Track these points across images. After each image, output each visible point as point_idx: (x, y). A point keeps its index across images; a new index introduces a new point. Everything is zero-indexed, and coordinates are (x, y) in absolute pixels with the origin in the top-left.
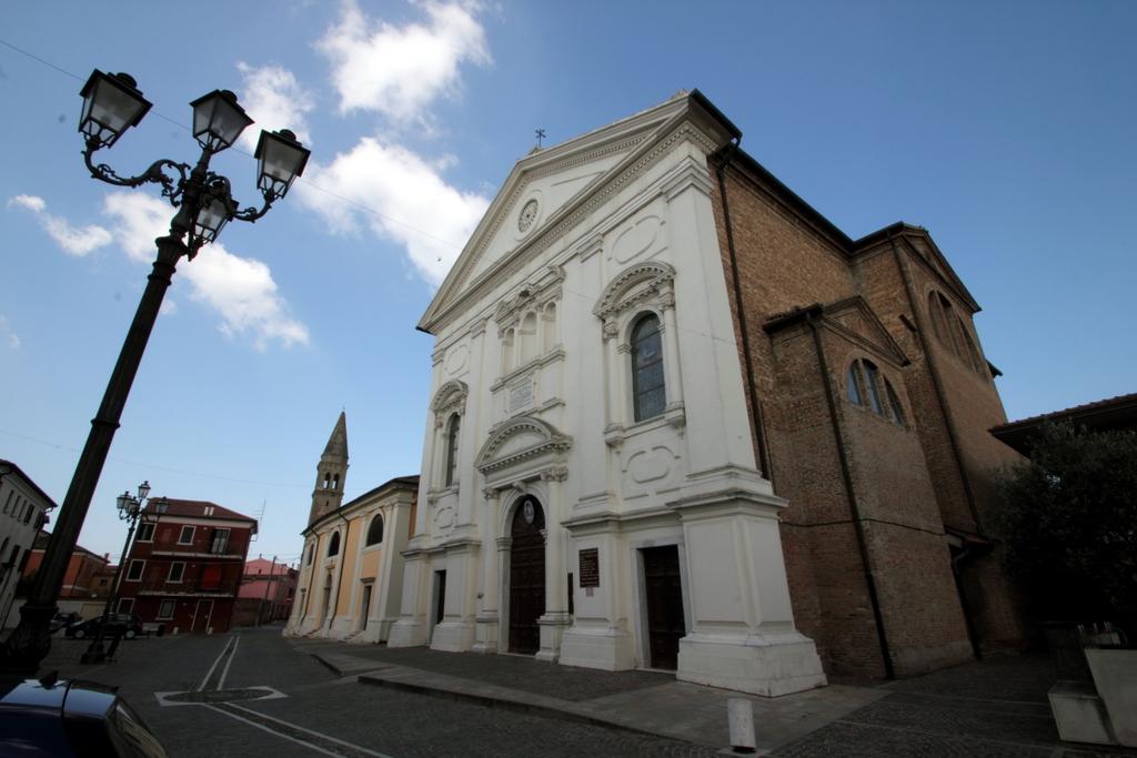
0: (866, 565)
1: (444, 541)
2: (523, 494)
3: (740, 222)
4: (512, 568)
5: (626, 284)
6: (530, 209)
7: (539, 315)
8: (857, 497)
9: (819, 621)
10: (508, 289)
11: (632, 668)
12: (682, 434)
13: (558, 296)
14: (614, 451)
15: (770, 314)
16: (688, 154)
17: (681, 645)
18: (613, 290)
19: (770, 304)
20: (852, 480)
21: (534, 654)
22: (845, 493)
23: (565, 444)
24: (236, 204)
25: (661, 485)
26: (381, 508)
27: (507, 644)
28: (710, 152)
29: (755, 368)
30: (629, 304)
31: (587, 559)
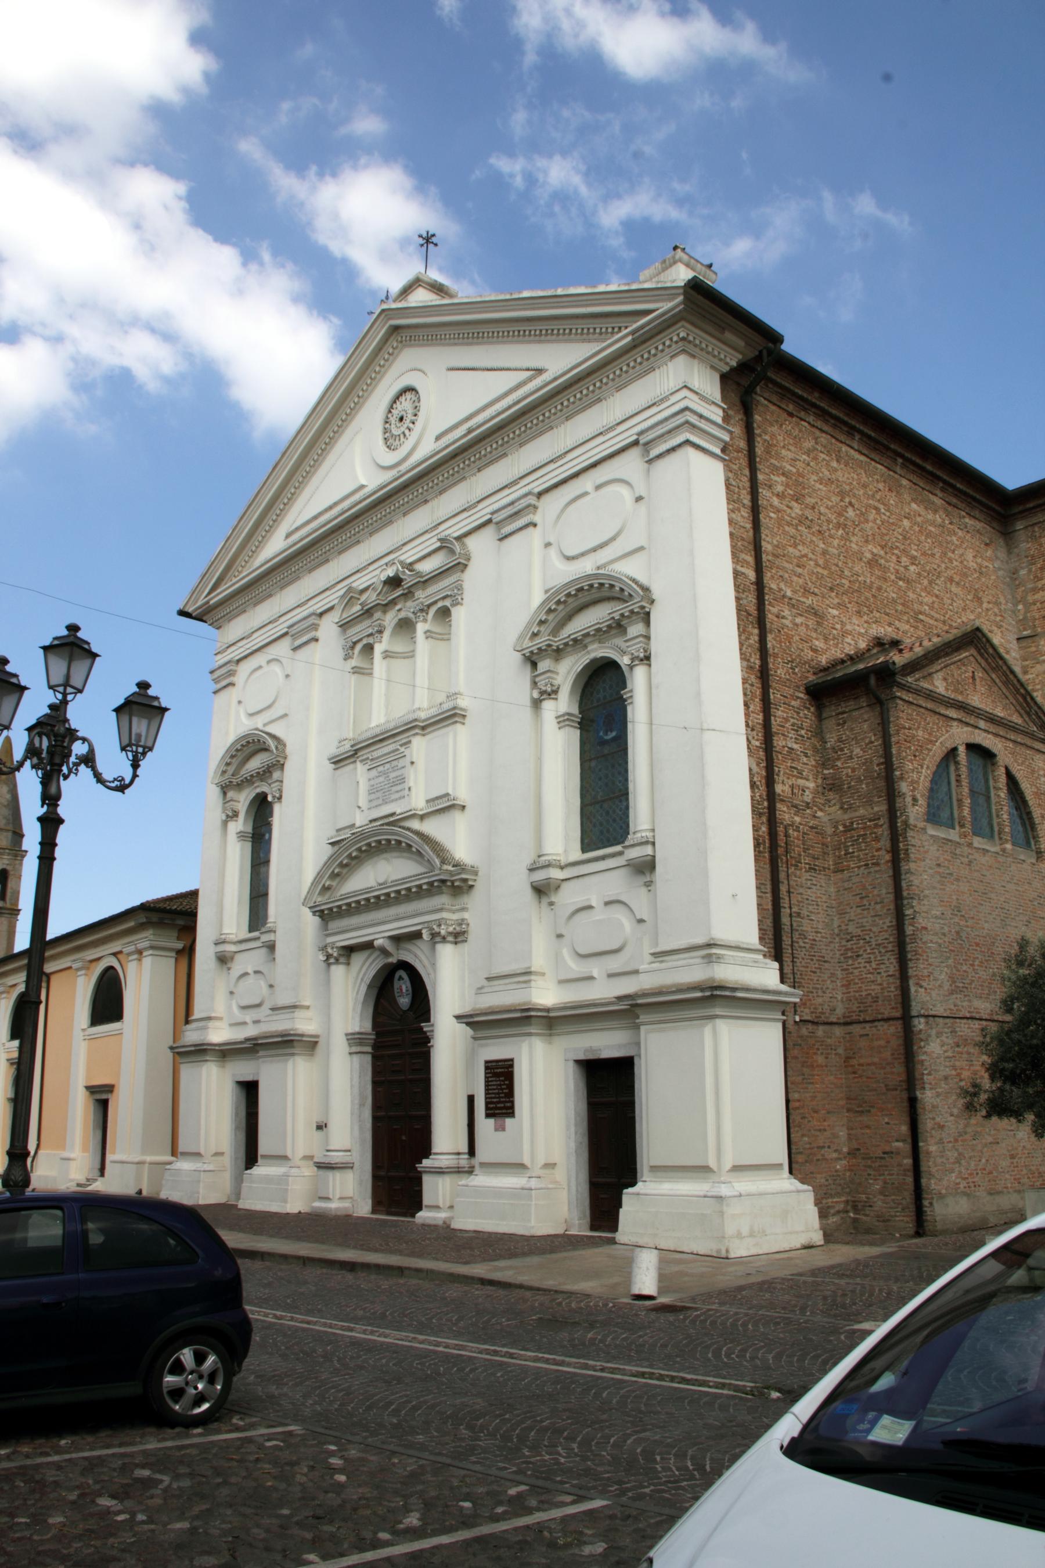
0: (911, 1083)
1: (251, 1031)
2: (393, 960)
3: (780, 488)
4: (375, 1083)
5: (573, 603)
6: (405, 404)
7: (421, 628)
8: (911, 982)
9: (844, 1162)
10: (364, 562)
11: (560, 1231)
12: (649, 884)
13: (455, 597)
14: (545, 901)
15: (824, 660)
16: (687, 382)
17: (625, 1199)
18: (550, 611)
19: (826, 639)
20: (909, 956)
21: (413, 1216)
22: (897, 974)
23: (465, 880)
24: (51, 707)
25: (615, 964)
26: (115, 954)
27: (370, 1202)
28: (726, 369)
29: (782, 768)
30: (578, 643)
31: (496, 1075)
